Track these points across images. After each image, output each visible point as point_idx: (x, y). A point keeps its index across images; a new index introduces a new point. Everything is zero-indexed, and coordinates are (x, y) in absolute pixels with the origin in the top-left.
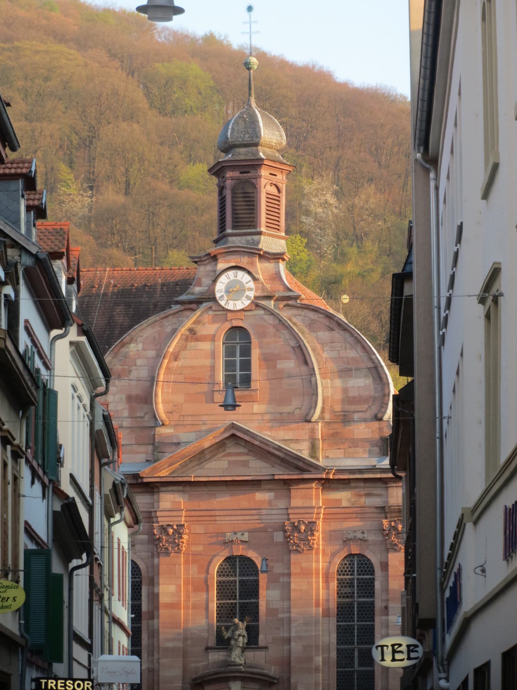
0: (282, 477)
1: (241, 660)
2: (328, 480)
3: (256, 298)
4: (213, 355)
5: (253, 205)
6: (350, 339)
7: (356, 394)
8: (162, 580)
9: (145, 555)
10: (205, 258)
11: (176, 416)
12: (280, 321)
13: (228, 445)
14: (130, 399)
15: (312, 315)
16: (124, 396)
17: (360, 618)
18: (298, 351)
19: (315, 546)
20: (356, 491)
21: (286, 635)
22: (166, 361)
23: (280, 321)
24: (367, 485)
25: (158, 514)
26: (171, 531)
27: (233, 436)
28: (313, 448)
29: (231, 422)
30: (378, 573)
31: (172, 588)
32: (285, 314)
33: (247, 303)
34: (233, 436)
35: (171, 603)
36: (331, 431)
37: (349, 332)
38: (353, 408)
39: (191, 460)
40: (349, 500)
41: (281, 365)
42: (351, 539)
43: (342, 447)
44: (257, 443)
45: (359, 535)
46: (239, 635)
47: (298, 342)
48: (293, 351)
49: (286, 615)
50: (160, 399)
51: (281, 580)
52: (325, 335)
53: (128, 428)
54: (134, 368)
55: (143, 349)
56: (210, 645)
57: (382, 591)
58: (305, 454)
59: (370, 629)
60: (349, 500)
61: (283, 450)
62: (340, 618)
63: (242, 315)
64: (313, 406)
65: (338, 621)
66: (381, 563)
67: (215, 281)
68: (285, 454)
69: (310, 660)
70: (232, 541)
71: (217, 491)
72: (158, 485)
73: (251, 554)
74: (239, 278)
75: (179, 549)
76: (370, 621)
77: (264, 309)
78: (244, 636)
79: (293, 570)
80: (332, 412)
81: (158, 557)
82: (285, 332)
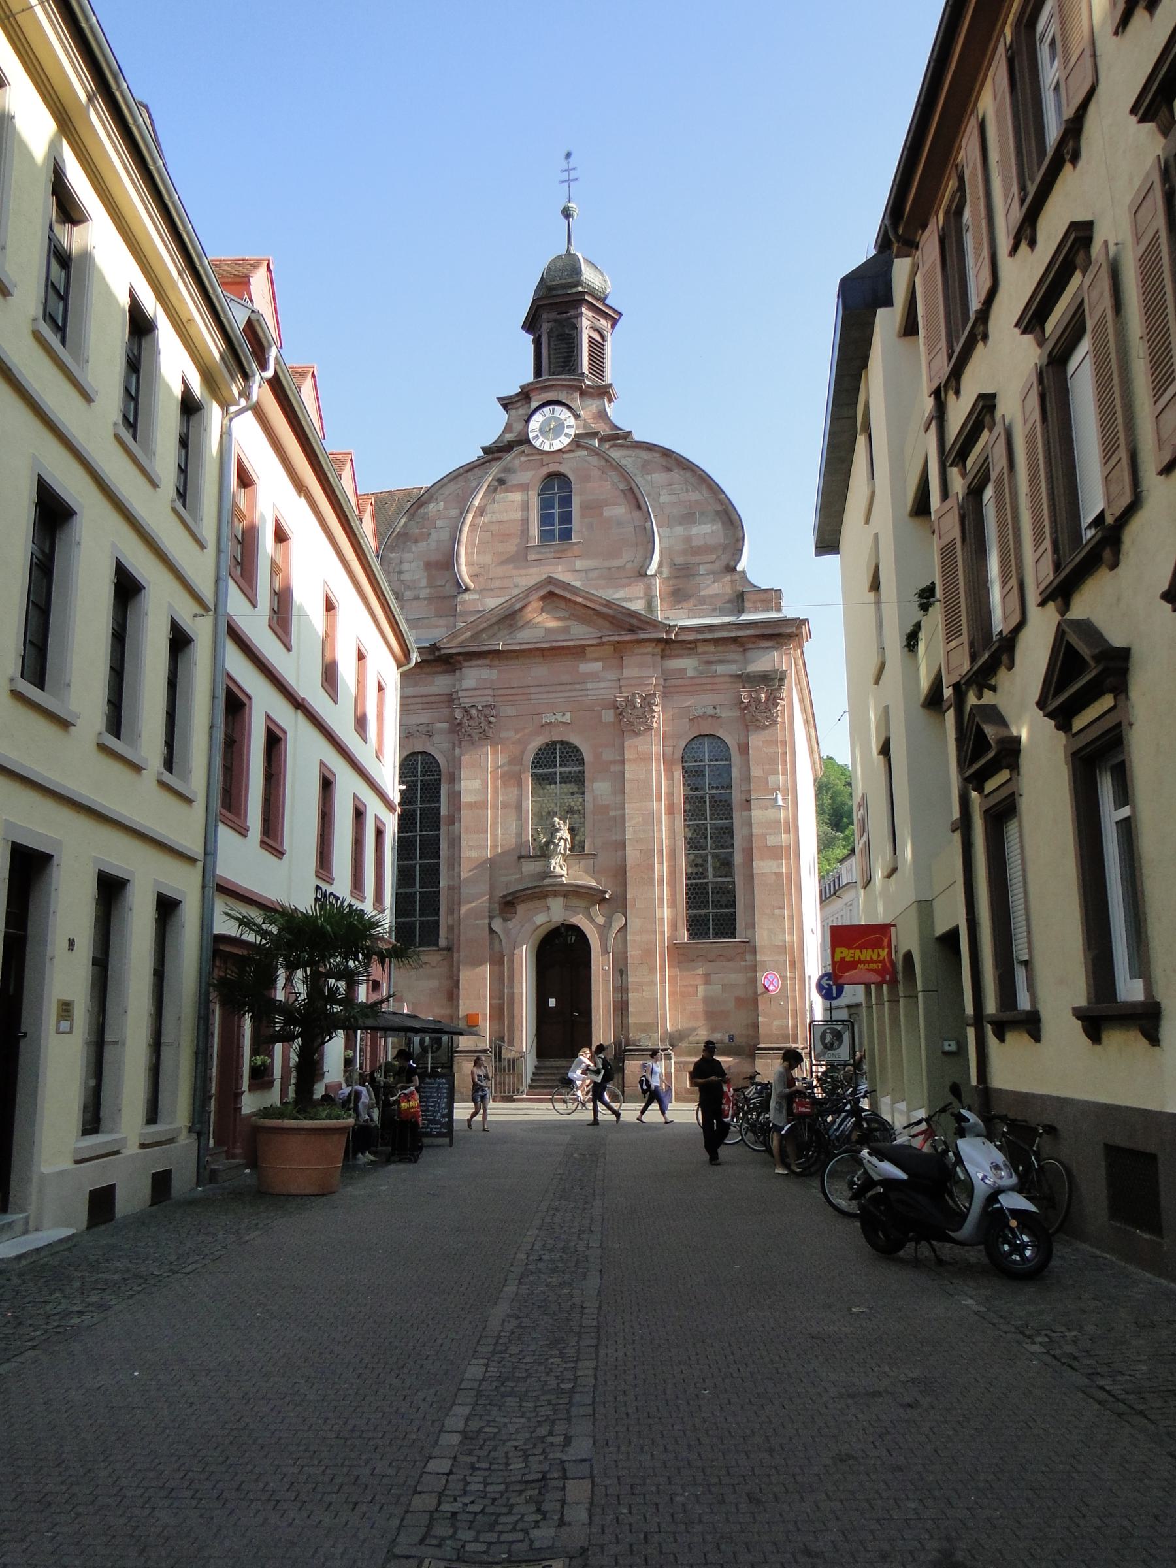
0: (611, 639)
2: (668, 642)
3: (577, 435)
4: (525, 506)
5: (573, 343)
6: (693, 480)
7: (702, 543)
8: (464, 773)
9: (445, 746)
10: (516, 399)
12: (607, 461)
14: (428, 565)
15: (645, 455)
16: (422, 563)
17: (713, 814)
18: (629, 494)
19: (655, 725)
21: (619, 838)
22: (470, 516)
23: (607, 461)
24: (719, 649)
25: (460, 694)
26: (474, 712)
27: (551, 594)
28: (650, 606)
29: (546, 576)
30: (736, 758)
31: (477, 784)
32: (615, 454)
33: (566, 441)
34: (551, 594)
37: (692, 471)
38: (697, 559)
39: (498, 622)
40: (695, 669)
41: (608, 512)
42: (700, 716)
43: (685, 605)
44: (580, 600)
45: (710, 711)
46: (560, 839)
47: (629, 483)
48: (622, 495)
49: (619, 813)
50: (462, 560)
52: (659, 477)
53: (425, 599)
54: (433, 530)
55: (445, 508)
58: (638, 606)
59: (703, 920)
60: (695, 669)
62: (688, 816)
63: (557, 458)
64: (649, 555)
66: (739, 745)
67: (527, 421)
72: (461, 658)
73: (575, 740)
74: (556, 414)
76: (726, 819)
77: (587, 449)
78: (566, 840)
79: (627, 755)
81: (460, 747)
82: (613, 474)
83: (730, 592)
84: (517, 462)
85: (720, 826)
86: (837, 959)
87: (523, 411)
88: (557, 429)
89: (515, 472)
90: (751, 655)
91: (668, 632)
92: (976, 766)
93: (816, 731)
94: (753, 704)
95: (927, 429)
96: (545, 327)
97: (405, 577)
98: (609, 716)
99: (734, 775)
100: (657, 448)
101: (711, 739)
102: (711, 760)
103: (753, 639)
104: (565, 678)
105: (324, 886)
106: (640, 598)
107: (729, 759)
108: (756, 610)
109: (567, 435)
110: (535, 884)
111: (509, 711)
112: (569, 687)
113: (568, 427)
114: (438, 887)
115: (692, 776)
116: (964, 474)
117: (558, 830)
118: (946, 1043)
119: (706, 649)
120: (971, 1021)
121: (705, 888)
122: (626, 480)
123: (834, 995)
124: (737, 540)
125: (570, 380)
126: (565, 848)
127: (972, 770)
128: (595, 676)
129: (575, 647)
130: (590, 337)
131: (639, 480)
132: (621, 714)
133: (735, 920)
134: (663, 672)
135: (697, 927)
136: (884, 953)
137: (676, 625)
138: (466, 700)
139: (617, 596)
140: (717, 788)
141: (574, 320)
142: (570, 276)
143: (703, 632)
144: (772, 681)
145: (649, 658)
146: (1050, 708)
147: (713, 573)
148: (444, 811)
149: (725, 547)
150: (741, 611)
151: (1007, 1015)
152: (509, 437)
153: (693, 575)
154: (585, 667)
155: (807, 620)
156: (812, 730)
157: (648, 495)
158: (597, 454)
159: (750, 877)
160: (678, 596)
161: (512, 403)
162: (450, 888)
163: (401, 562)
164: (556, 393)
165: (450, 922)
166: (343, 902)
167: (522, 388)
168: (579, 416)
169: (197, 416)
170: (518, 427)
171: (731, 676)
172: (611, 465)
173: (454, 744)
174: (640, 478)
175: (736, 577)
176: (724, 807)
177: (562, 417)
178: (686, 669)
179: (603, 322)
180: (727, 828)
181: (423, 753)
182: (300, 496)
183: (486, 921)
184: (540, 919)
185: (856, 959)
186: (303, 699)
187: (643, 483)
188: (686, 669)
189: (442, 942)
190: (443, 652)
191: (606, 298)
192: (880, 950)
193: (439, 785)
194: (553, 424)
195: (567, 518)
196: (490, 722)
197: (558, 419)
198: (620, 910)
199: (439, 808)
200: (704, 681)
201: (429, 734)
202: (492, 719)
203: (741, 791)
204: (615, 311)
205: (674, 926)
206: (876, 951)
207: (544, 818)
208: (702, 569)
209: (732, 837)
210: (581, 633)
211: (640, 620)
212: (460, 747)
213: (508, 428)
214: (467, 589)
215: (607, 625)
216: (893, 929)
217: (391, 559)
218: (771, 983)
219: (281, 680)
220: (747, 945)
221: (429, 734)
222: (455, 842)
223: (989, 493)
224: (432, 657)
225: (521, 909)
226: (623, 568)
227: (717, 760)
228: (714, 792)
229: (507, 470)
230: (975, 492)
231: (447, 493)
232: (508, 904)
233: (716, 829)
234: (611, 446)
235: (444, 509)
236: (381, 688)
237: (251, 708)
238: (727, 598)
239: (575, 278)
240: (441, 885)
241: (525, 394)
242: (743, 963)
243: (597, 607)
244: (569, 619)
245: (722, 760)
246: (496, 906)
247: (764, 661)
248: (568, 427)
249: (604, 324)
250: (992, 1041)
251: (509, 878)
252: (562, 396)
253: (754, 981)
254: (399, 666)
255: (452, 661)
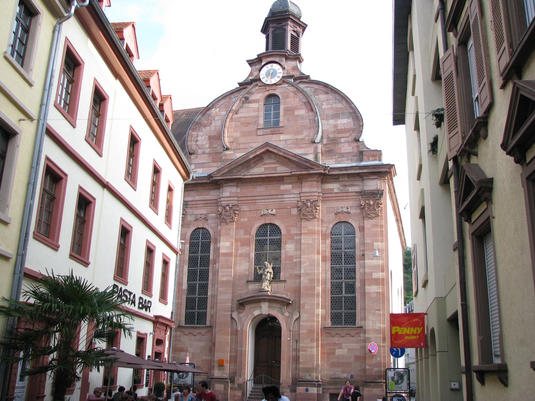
0: (296, 173)
1: (268, 288)
2: (324, 175)
3: (283, 77)
8: (222, 238)
9: (213, 225)
11: (235, 144)
12: (297, 89)
13: (265, 158)
14: (210, 138)
15: (316, 86)
16: (207, 137)
18: (307, 104)
20: (343, 183)
21: (298, 272)
23: (297, 89)
26: (228, 208)
28: (316, 157)
30: (358, 234)
31: (228, 244)
32: (302, 86)
35: (227, 253)
36: (327, 149)
38: (340, 135)
40: (338, 189)
42: (340, 212)
44: (281, 154)
45: (345, 210)
46: (268, 272)
47: (307, 99)
48: (304, 105)
49: (298, 260)
51: (295, 238)
52: (323, 97)
53: (207, 154)
54: (213, 121)
55: (219, 111)
56: (250, 279)
57: (360, 245)
58: (311, 157)
61: (297, 157)
63: (274, 87)
65: (331, 264)
66: (359, 227)
67: (260, 71)
68: (299, 159)
69: (313, 288)
70: (266, 214)
71: (257, 185)
72: (222, 182)
74: (274, 67)
75: (232, 220)
78: (270, 273)
79: (303, 231)
80: (328, 138)
83: (356, 151)
84: (254, 89)
85: (349, 268)
86: (393, 333)
87: (258, 67)
88: (273, 74)
89: (253, 94)
90: (365, 182)
91: (324, 170)
92: (466, 203)
93: (402, 225)
94: (366, 206)
95: (436, 21)
96: (271, 30)
97: (198, 143)
98: (295, 211)
99: (356, 242)
100: (321, 83)
101: (345, 224)
102: (346, 235)
103: (367, 174)
104: (273, 192)
105: (120, 285)
106: (312, 154)
107: (354, 234)
108: (369, 160)
109: (278, 77)
110: (257, 295)
111: (245, 208)
112: (275, 197)
113: (279, 73)
114: (207, 295)
115: (335, 242)
116: (456, 36)
117: (267, 268)
118: (453, 384)
119: (344, 179)
120: (464, 370)
121: (340, 300)
122: (306, 97)
123: (400, 355)
124: (360, 126)
125: (281, 52)
126: (270, 278)
127: (463, 208)
128: (288, 192)
129: (279, 177)
130: (291, 34)
131: (313, 98)
132: (300, 210)
133: (355, 316)
134: (322, 190)
135: (336, 318)
136: (420, 330)
137: (329, 167)
138: (224, 202)
139: (300, 153)
140: (348, 248)
141: (285, 27)
142: (283, 7)
143: (342, 170)
144: (377, 195)
145: (315, 183)
146: (509, 148)
147: (348, 142)
148: (211, 257)
149: (354, 130)
150: (361, 160)
151: (485, 367)
152: (251, 78)
153: (337, 143)
154: (284, 187)
155: (394, 165)
156: (400, 225)
157: (317, 105)
158: (293, 86)
159: (364, 294)
160: (329, 152)
161: (253, 63)
162: (212, 296)
163: (197, 136)
164: (274, 58)
165: (212, 313)
166: (134, 296)
167: (258, 55)
168: (285, 68)
169: (36, 17)
170: (255, 74)
171: (356, 192)
172: (299, 90)
173: (218, 224)
174: (313, 97)
175: (359, 144)
176: (351, 258)
177: (276, 69)
178: (333, 189)
179: (298, 28)
180: (352, 269)
181: (203, 228)
182: (116, 79)
183: (230, 313)
184: (257, 313)
185: (404, 333)
186: (108, 182)
187: (314, 99)
188: (333, 189)
189: (208, 323)
190: (214, 178)
191: (300, 18)
192: (418, 328)
193: (210, 244)
194: (272, 71)
195: (277, 115)
196: (235, 214)
197: (274, 70)
198: (297, 309)
199: (209, 256)
200: (343, 194)
201: (206, 219)
202: (236, 212)
203: (360, 250)
204: (304, 24)
205: (324, 318)
206: (416, 328)
207: (259, 260)
208: (342, 140)
209: (355, 274)
210: (282, 170)
211: (311, 164)
212: (221, 225)
213: (251, 74)
214: (227, 149)
215: (294, 166)
216: (426, 316)
217: (193, 135)
218: (373, 348)
219: (94, 172)
220: (361, 329)
221: (206, 219)
222: (216, 273)
223: (471, 42)
224: (209, 181)
225: (247, 307)
226: (304, 139)
227: (348, 234)
228: (346, 250)
229: (249, 93)
230: (463, 43)
231: (221, 104)
232: (242, 304)
233: (347, 269)
234: (300, 82)
235: (219, 111)
236: (170, 189)
237: (66, 181)
238: (354, 154)
239: (286, 9)
240: (208, 294)
241: (260, 58)
242: (358, 338)
243: (290, 157)
244: (276, 163)
245: (351, 234)
246: (235, 306)
247: (372, 185)
248: (279, 73)
249: (299, 29)
250: (477, 384)
251: (241, 292)
252: (277, 60)
253: (364, 347)
254: (184, 180)
255: (218, 183)
